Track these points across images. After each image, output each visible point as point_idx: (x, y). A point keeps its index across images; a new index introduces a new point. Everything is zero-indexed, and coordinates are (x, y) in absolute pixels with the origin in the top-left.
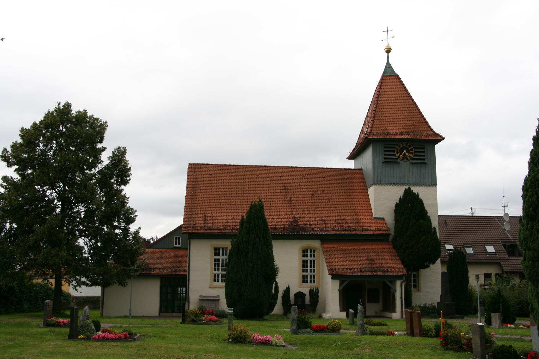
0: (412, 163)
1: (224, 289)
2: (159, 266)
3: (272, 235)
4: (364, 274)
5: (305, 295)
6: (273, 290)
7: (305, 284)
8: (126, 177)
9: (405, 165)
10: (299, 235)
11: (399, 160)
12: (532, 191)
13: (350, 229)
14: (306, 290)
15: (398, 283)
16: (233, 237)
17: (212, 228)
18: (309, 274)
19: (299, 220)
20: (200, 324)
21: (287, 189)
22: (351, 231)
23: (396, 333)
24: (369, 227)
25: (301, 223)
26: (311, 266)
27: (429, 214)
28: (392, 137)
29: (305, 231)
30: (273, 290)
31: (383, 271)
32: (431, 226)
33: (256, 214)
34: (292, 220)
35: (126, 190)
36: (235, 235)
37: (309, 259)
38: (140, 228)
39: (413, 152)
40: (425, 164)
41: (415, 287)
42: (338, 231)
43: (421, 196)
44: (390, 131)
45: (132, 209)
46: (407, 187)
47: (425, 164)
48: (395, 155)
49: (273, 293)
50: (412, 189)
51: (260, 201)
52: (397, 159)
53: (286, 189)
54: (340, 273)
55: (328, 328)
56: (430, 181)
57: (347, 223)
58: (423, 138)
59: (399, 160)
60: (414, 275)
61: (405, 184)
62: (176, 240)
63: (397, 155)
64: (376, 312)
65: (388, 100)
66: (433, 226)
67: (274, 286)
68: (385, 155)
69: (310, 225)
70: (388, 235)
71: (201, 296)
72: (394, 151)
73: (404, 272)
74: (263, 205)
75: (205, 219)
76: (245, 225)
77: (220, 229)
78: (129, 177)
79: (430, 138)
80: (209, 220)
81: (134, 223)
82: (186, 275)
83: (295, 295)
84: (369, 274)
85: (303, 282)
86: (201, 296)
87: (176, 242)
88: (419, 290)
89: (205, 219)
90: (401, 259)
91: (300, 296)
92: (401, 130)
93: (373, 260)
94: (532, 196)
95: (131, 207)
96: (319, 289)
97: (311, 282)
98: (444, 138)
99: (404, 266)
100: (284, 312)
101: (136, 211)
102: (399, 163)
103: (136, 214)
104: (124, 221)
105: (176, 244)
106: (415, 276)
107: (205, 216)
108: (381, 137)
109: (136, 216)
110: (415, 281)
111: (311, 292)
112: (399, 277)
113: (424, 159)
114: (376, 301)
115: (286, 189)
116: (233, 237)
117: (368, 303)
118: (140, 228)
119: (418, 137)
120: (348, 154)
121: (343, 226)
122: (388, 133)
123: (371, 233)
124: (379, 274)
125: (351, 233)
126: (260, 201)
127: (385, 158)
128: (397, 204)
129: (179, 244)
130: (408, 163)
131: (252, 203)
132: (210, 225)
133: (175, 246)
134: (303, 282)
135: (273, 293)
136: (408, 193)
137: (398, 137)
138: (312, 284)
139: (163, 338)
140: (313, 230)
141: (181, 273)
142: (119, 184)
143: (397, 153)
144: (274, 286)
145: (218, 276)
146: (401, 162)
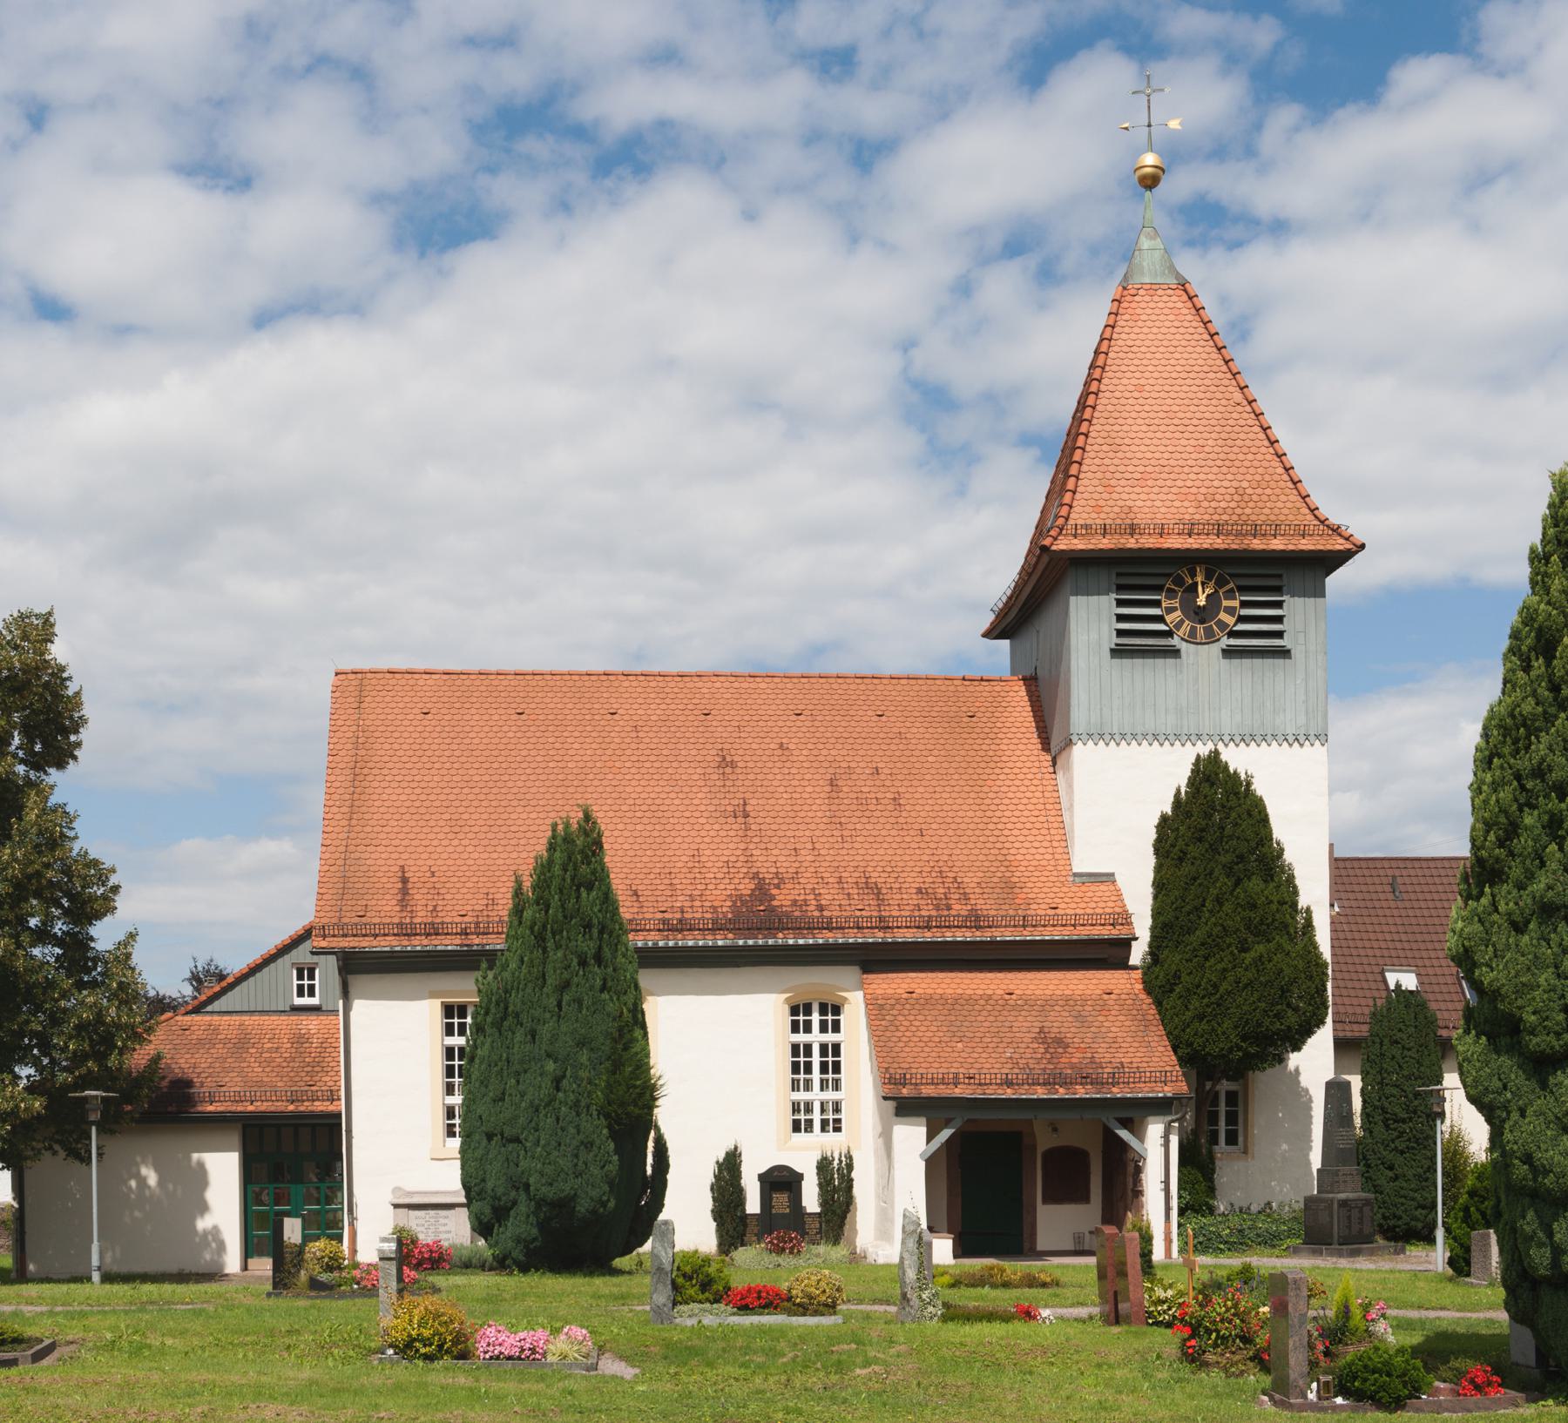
0: (1229, 653)
1: (458, 1163)
2: (233, 1084)
3: (638, 950)
4: (1024, 1094)
5: (800, 1177)
6: (650, 1160)
7: (802, 1137)
8: (66, 732)
9: (1202, 660)
10: (775, 948)
11: (1176, 641)
12: (1502, 767)
13: (975, 920)
14: (802, 1155)
15: (1155, 1130)
16: (484, 965)
17: (434, 931)
18: (816, 1095)
19: (777, 887)
20: (342, 1296)
21: (733, 765)
22: (978, 928)
23: (1045, 1313)
24: (1056, 914)
25: (782, 899)
26: (824, 1068)
27: (1288, 857)
28: (1149, 542)
29: (798, 930)
30: (650, 1160)
31: (1097, 1083)
32: (1295, 904)
33: (573, 871)
34: (747, 887)
35: (64, 785)
36: (490, 956)
37: (816, 1038)
38: (132, 936)
39: (1236, 603)
40: (1284, 653)
41: (1232, 1139)
42: (929, 928)
43: (1259, 788)
44: (1141, 519)
45: (95, 863)
46: (1204, 749)
47: (1284, 653)
48: (1159, 619)
49: (649, 1171)
50: (1224, 757)
51: (587, 817)
52: (1169, 634)
53: (726, 763)
54: (928, 1091)
55: (789, 1299)
56: (1302, 720)
57: (966, 897)
58: (1277, 544)
59: (1176, 641)
60: (1228, 1093)
61: (1199, 737)
62: (300, 977)
63: (1168, 618)
64: (1078, 1238)
65: (1140, 388)
66: (1302, 902)
67: (651, 1144)
68: (1120, 618)
69: (821, 908)
70: (1125, 944)
71: (396, 1190)
72: (1157, 604)
73: (1175, 1084)
74: (600, 835)
75: (404, 891)
76: (528, 914)
77: (465, 933)
78: (76, 732)
79: (1306, 545)
80: (419, 897)
81: (108, 919)
82: (339, 1115)
83: (761, 1177)
84: (1040, 1093)
85: (796, 1127)
86: (396, 1190)
87: (301, 988)
88: (1245, 1152)
89: (404, 891)
90: (1169, 1034)
91: (781, 1181)
92: (1190, 512)
93: (1059, 1041)
94: (1496, 786)
95: (93, 855)
96: (854, 1154)
97: (824, 1127)
98: (1363, 546)
99: (1182, 1061)
100: (720, 1245)
101: (113, 871)
102: (1175, 653)
103: (114, 880)
104: (66, 912)
105: (301, 994)
106: (1232, 1098)
107: (405, 880)
108: (1105, 543)
109: (116, 889)
110: (1232, 1118)
111: (824, 1166)
112: (1159, 1106)
113: (1279, 635)
114: (1079, 1195)
115: (726, 763)
116: (484, 965)
117: (1046, 1201)
118: (132, 936)
119: (1257, 544)
120: (988, 619)
121: (949, 908)
122: (1133, 530)
123: (1057, 934)
124: (1081, 1092)
125: (978, 936)
126: (587, 817)
127: (1120, 633)
128: (1164, 819)
129: (312, 994)
130: (1215, 650)
131: (554, 826)
132: (421, 916)
133: (298, 1001)
134: (796, 1127)
135: (649, 1171)
136: (1209, 773)
137: (1175, 542)
138: (831, 1136)
139: (137, 1351)
140: (830, 929)
141: (320, 1106)
142: (38, 763)
143: (1170, 610)
144: (651, 1144)
145: (809, 1108)
146: (1183, 646)
